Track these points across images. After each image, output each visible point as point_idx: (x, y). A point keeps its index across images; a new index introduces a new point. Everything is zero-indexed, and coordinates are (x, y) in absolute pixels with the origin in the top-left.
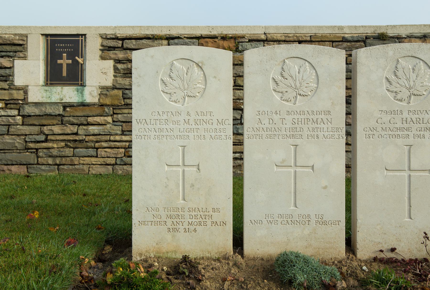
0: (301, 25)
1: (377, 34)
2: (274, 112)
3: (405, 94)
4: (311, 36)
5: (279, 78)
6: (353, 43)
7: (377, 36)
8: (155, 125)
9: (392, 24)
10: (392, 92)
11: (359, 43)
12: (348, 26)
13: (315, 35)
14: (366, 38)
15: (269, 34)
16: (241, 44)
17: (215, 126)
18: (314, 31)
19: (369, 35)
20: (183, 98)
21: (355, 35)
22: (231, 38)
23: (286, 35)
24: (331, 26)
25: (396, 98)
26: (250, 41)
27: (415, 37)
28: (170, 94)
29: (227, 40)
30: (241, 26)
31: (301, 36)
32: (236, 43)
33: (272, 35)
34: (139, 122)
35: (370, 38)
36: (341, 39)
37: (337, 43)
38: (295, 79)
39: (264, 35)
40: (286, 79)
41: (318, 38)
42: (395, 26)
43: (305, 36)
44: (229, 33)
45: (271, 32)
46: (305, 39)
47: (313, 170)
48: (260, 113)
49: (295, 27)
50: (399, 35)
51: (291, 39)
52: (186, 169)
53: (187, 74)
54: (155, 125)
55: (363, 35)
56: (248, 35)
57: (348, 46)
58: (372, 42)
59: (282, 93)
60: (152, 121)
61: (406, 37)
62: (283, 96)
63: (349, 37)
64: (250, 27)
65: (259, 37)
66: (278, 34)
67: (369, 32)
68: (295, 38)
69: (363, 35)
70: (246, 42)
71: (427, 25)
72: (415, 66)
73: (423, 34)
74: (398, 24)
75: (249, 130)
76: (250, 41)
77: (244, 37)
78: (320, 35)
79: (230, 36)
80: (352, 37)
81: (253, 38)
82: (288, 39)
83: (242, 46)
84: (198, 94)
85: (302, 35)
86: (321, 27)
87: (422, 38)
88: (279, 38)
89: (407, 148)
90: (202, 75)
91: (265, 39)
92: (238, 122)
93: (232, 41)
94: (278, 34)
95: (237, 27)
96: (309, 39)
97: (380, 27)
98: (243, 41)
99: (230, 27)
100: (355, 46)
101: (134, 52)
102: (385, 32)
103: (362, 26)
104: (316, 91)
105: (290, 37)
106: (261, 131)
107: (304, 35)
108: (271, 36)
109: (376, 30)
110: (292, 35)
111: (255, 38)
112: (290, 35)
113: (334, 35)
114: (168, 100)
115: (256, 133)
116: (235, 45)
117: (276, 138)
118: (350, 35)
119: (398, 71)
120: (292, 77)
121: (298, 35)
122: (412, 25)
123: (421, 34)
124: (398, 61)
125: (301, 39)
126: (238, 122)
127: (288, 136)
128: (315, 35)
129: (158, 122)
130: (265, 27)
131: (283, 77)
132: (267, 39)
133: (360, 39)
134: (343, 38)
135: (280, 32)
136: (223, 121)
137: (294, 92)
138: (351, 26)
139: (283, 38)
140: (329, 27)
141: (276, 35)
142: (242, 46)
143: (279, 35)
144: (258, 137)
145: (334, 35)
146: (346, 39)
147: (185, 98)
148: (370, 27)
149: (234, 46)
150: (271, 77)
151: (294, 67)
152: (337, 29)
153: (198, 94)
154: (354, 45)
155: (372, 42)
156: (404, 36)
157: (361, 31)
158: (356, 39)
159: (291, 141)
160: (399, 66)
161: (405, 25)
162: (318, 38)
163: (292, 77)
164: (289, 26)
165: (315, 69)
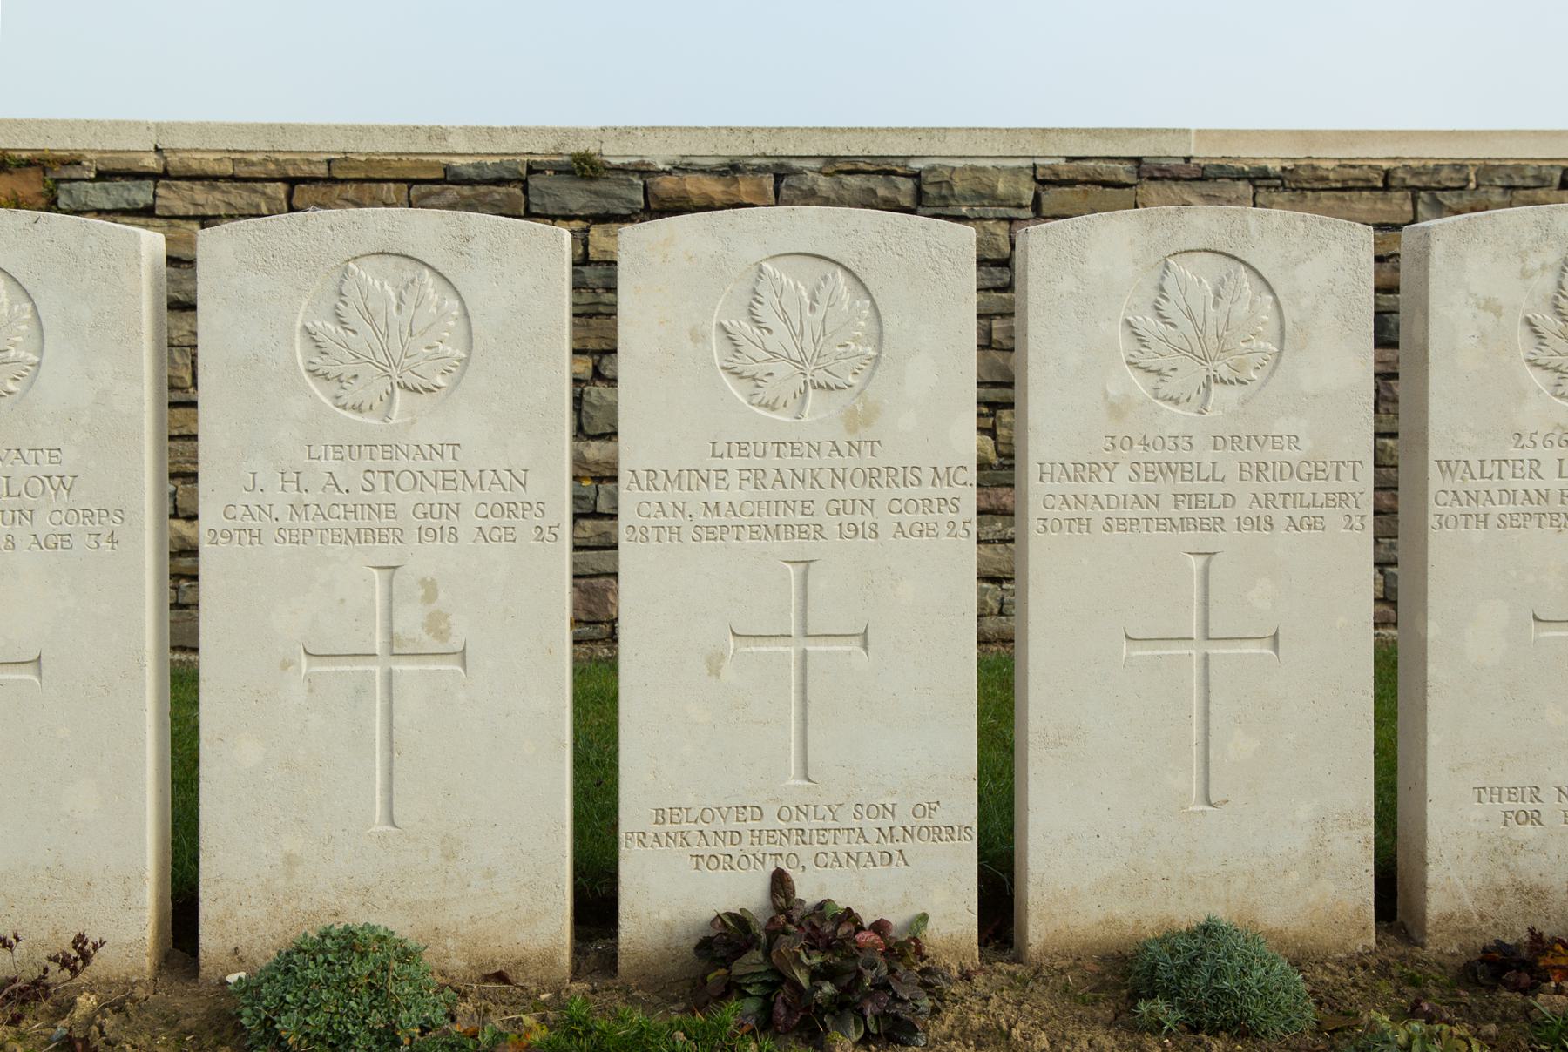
0: (293, 121)
1: (566, 159)
2: (1137, 438)
3: (1188, 376)
4: (329, 162)
5: (327, 328)
6: (482, 189)
7: (568, 164)
8: (1495, 479)
9: (620, 124)
10: (1147, 370)
11: (502, 190)
12: (465, 128)
13: (346, 159)
14: (532, 170)
15: (174, 151)
16: (64, 186)
17: (927, 490)
18: (338, 145)
19: (538, 159)
20: (385, 396)
21: (489, 161)
22: (29, 163)
23: (238, 156)
24: (403, 128)
25: (1161, 394)
26: (102, 176)
27: (703, 171)
28: (753, 378)
29: (11, 173)
30: (65, 123)
31: (294, 163)
32: (590, 195)
33: (186, 155)
34: (1447, 468)
35: (542, 172)
36: (440, 175)
37: (424, 188)
38: (1200, 322)
39: (154, 156)
40: (769, 331)
41: (355, 169)
42: (628, 132)
43: (309, 162)
44: (20, 146)
45: (179, 145)
46: (306, 170)
47: (464, 666)
48: (1117, 442)
49: (268, 129)
50: (643, 163)
51: (257, 171)
52: (812, 647)
53: (399, 308)
54: (1495, 479)
55: (518, 159)
56: (93, 156)
57: (463, 197)
58: (547, 183)
59: (1159, 372)
60: (1487, 465)
61: (668, 168)
62: (1161, 384)
63: (468, 165)
64: (101, 124)
65: (136, 161)
66: (209, 151)
67: (540, 148)
68: (272, 167)
69: (518, 159)
70: (90, 180)
71: (739, 129)
72: (1222, 282)
73: (727, 161)
74: (639, 125)
75: (1442, 497)
76: (102, 176)
77: (79, 163)
78: (363, 158)
79: (24, 155)
80: (478, 166)
81: (111, 166)
82: (243, 171)
83: (69, 192)
84: (851, 380)
85: (297, 157)
86: (366, 130)
87: (726, 172)
88: (211, 167)
89: (1196, 563)
90: (866, 312)
91: (161, 170)
92: (999, 472)
93: (32, 174)
94: (209, 151)
95: (51, 122)
96: (322, 171)
97: (577, 133)
98: (75, 175)
99: (21, 123)
100: (488, 199)
101: (628, 232)
102: (593, 150)
103: (515, 130)
104: (1277, 361)
105: (253, 164)
106: (1481, 500)
107: (304, 156)
108: (181, 160)
109: (562, 144)
110: (261, 157)
111: (119, 166)
112: (254, 158)
113: (413, 158)
114: (744, 401)
115: (1074, 513)
116: (42, 189)
117: (730, 538)
118: (470, 160)
119: (1167, 299)
120: (1191, 317)
121: (281, 157)
122: (689, 129)
123: (720, 161)
124: (1167, 266)
125: (291, 173)
126: (999, 472)
127: (772, 528)
128: (346, 159)
129: (1507, 470)
130: (157, 125)
131: (1161, 316)
132: (166, 170)
133: (507, 175)
134: (447, 168)
135: (214, 147)
136: (952, 471)
137: (1189, 371)
138: (473, 129)
139: (228, 169)
140: (394, 129)
141: (198, 156)
142: (69, 192)
143: (211, 156)
144: (1472, 521)
145: (413, 158)
146: (456, 174)
147: (391, 395)
148: (541, 131)
149: (41, 194)
150: (299, 325)
151: (1200, 282)
152: (423, 137)
153: (851, 380)
154: (485, 195)
155: (547, 183)
156: (661, 167)
157: (509, 145)
158: (490, 174)
159: (1190, 538)
160: (1169, 284)
161: (664, 128)
162: (355, 169)
163: (1191, 317)
164: (248, 126)
165: (1272, 292)
